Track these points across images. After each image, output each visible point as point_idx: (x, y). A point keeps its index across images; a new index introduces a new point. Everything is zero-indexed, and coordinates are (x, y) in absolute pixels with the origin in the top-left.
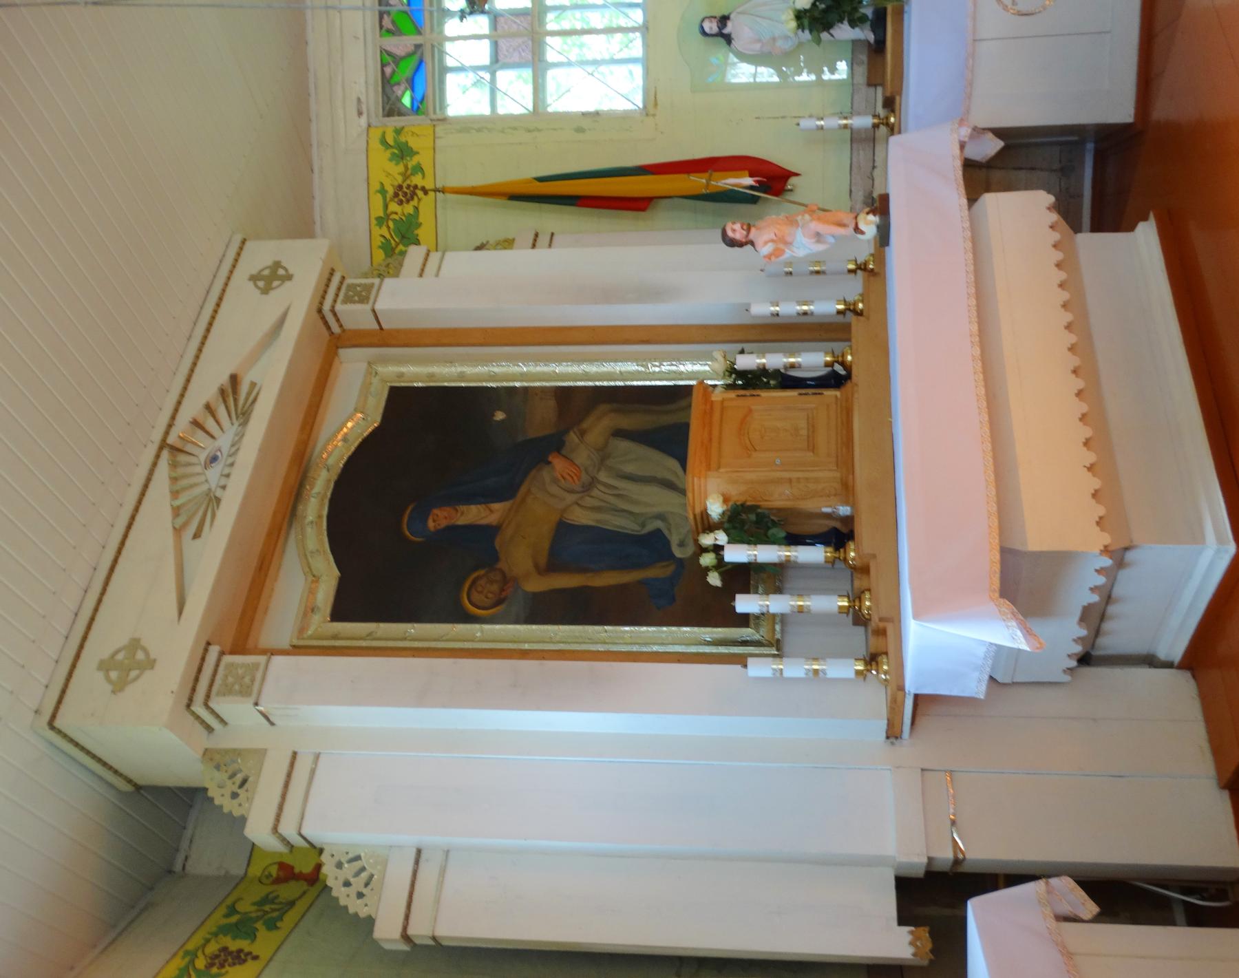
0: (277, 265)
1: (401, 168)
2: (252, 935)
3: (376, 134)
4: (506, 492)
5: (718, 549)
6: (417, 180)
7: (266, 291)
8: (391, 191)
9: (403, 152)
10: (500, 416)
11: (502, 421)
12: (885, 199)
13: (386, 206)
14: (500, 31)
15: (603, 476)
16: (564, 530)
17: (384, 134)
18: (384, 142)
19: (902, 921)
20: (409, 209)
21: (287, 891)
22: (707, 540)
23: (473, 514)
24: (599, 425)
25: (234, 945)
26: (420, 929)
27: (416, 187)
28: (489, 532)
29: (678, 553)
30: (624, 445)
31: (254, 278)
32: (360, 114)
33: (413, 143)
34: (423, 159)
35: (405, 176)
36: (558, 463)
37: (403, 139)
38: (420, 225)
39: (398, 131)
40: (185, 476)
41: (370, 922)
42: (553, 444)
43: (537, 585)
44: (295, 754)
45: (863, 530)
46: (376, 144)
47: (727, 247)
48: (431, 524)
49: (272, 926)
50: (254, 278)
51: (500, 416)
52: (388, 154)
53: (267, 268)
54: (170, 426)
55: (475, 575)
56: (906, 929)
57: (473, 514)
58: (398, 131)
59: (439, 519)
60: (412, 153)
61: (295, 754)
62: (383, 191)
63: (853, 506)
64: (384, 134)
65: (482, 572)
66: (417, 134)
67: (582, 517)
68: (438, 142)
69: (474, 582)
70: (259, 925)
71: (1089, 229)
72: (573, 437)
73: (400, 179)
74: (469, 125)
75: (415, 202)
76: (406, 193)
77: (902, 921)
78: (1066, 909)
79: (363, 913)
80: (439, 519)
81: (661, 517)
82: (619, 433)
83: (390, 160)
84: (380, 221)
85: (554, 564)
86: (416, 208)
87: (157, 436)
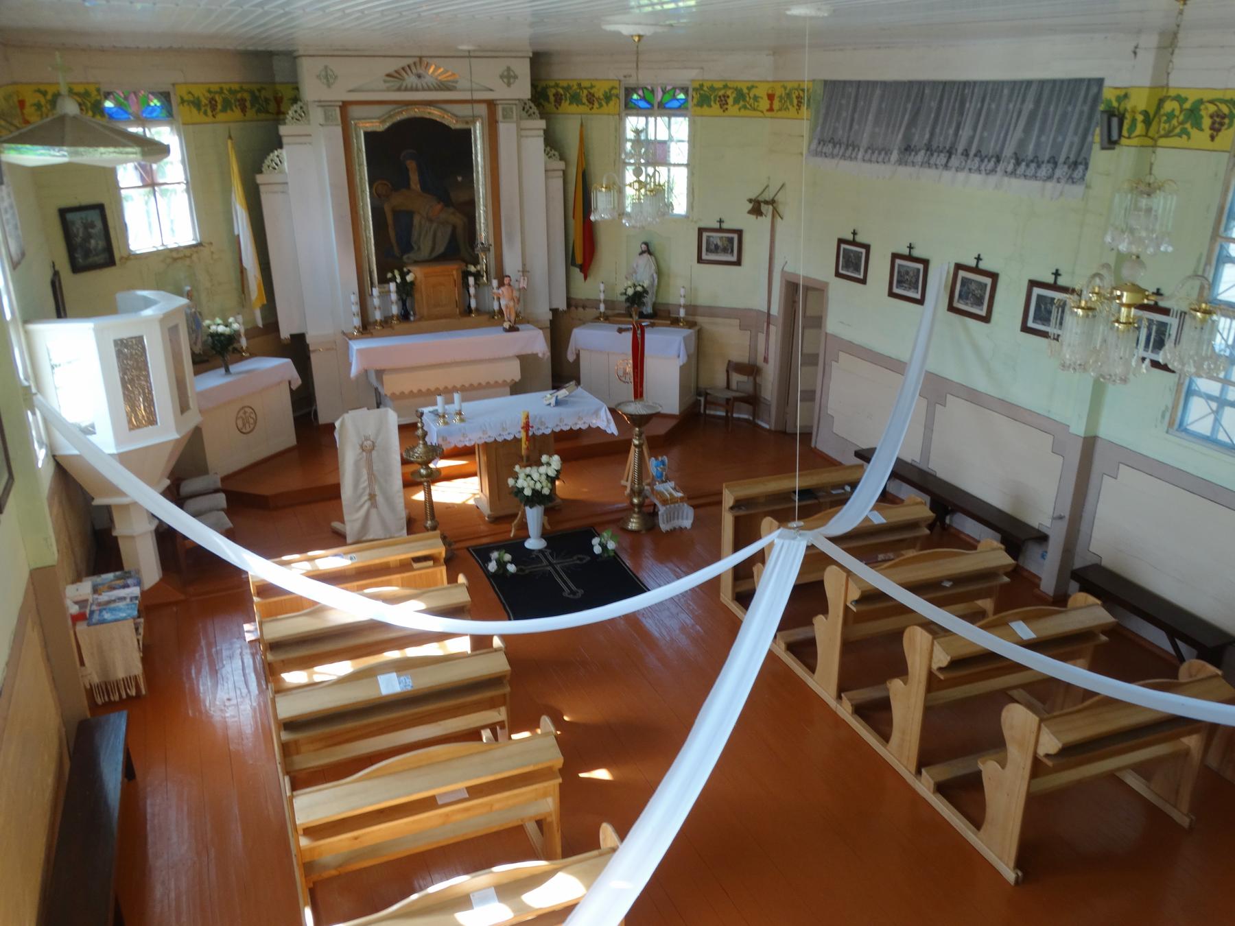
0: (516, 77)
1: (602, 97)
2: (252, 106)
3: (616, 84)
4: (425, 188)
5: (394, 279)
6: (596, 105)
7: (502, 77)
8: (592, 91)
9: (608, 98)
10: (460, 179)
11: (457, 180)
12: (517, 330)
13: (585, 88)
14: (658, 145)
15: (435, 225)
16: (410, 214)
17: (616, 88)
18: (613, 88)
19: (291, 336)
20: (585, 100)
21: (272, 107)
22: (396, 273)
23: (414, 178)
24: (458, 220)
25: (248, 104)
26: (262, 189)
27: (593, 104)
28: (408, 186)
29: (405, 257)
30: (449, 230)
31: (509, 69)
32: (625, 77)
33: (612, 103)
34: (605, 108)
35: (598, 99)
36: (439, 207)
37: (613, 98)
38: (577, 105)
39: (617, 96)
40: (406, 72)
41: (261, 172)
42: (446, 201)
43: (387, 208)
44: (310, 135)
45: (405, 326)
46: (611, 84)
47: (15, 480)
48: (408, 162)
49: (259, 111)
50: (509, 69)
51: (460, 179)
52: (607, 90)
53: (503, 81)
54: (431, 57)
55: (389, 184)
56: (289, 337)
57: (414, 178)
58: (617, 96)
59: (412, 165)
60: (607, 103)
61: (310, 135)
62: (592, 87)
63: (414, 321)
64: (616, 88)
65: (390, 186)
66: (613, 106)
67: (416, 220)
68: (611, 117)
69: (385, 184)
70: (257, 106)
71: (551, 387)
72: (451, 210)
73: (596, 95)
74: (620, 130)
75: (587, 103)
76: (591, 99)
77: (291, 336)
78: (292, 382)
79: (263, 169)
80: (412, 165)
81: (419, 249)
82: (454, 228)
83: (605, 91)
84: (579, 85)
85: (396, 213)
86: (584, 104)
87: (424, 54)
